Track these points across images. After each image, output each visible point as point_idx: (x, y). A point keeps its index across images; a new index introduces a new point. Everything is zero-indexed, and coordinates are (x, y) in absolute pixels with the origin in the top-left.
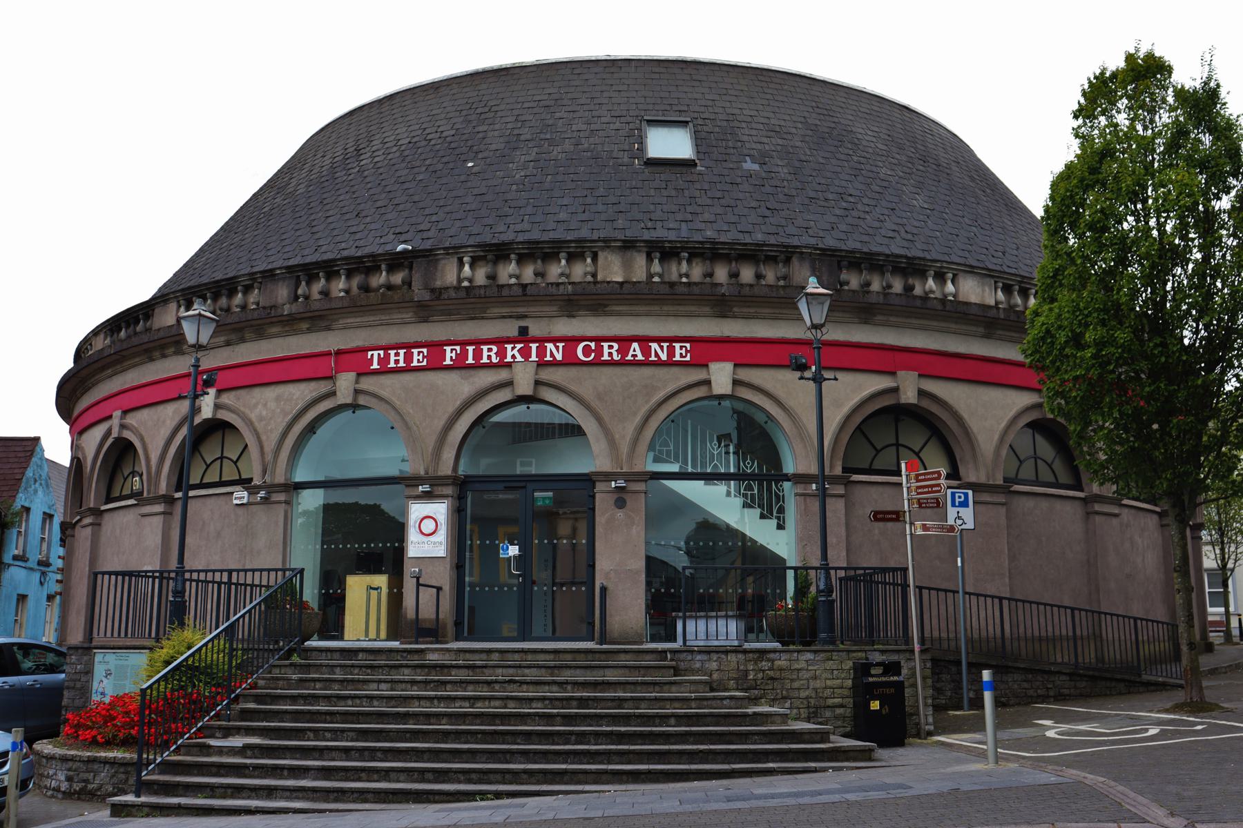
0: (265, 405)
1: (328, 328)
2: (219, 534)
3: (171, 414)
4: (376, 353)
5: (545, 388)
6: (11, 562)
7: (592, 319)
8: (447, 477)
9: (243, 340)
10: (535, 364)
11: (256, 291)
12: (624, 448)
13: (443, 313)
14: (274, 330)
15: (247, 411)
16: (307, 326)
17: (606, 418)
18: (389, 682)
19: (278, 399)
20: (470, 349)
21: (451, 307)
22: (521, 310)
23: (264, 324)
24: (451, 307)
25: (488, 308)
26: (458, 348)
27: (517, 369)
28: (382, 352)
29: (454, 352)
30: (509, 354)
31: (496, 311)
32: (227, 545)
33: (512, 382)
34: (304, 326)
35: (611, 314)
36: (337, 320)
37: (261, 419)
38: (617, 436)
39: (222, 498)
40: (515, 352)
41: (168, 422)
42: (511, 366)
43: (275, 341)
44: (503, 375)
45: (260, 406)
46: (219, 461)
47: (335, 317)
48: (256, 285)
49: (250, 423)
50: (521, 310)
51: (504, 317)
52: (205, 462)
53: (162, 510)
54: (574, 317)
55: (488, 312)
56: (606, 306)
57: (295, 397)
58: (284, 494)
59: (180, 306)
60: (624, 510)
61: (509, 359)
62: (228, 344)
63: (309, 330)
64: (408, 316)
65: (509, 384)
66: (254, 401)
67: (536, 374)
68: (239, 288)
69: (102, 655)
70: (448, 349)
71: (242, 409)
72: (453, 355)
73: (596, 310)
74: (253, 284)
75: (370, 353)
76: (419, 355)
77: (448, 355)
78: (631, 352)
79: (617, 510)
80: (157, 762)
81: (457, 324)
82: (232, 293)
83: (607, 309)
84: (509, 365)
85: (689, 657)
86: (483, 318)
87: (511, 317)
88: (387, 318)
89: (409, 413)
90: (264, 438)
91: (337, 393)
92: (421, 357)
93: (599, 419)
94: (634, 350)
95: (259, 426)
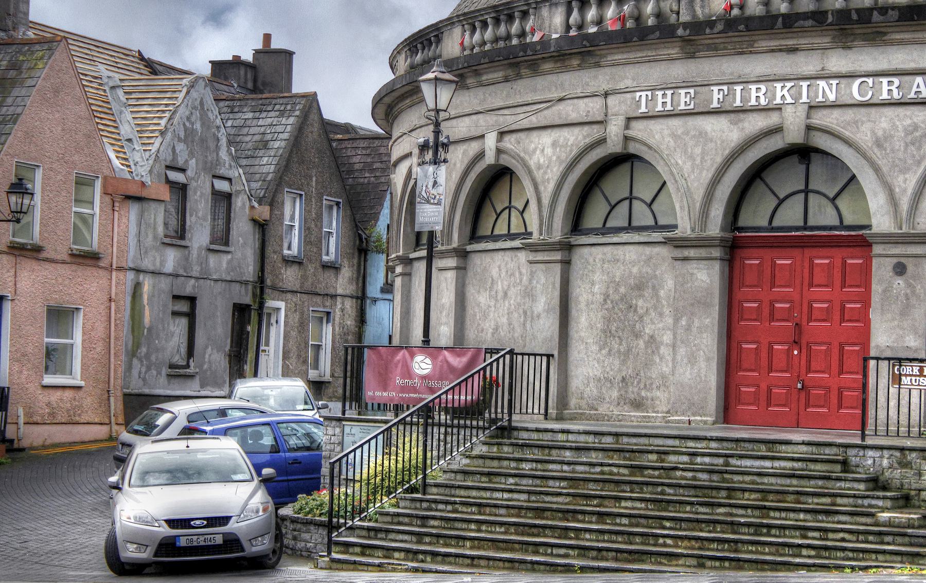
0: (543, 151)
1: (598, 65)
2: (506, 294)
3: (460, 156)
4: (644, 94)
5: (818, 134)
6: (379, 295)
7: (871, 50)
8: (713, 239)
9: (519, 76)
10: (806, 107)
11: (532, 17)
12: (905, 204)
13: (709, 47)
14: (547, 66)
15: (527, 158)
16: (578, 62)
17: (885, 169)
18: (722, 456)
19: (554, 144)
20: (738, 88)
21: (717, 41)
22: (790, 42)
23: (539, 59)
24: (717, 41)
25: (755, 41)
26: (725, 88)
27: (789, 111)
28: (649, 93)
29: (721, 93)
30: (779, 94)
31: (764, 44)
32: (513, 307)
33: (782, 127)
34: (575, 62)
35: (892, 43)
36: (605, 56)
37: (539, 167)
38: (897, 190)
39: (508, 253)
40: (785, 92)
41: (458, 165)
42: (781, 109)
43: (550, 78)
44: (773, 119)
45: (538, 152)
46: (507, 211)
47: (603, 52)
48: (531, 11)
49: (530, 172)
50: (790, 42)
51: (773, 51)
52: (496, 211)
53: (455, 265)
54: (849, 48)
55: (756, 45)
56: (885, 34)
57: (569, 144)
58: (560, 253)
59: (465, 31)
60: (904, 277)
61: (778, 101)
62: (506, 80)
63: (580, 67)
64: (674, 51)
65: (777, 130)
66: (533, 146)
67: (808, 117)
68: (516, 14)
69: (350, 427)
70: (715, 89)
71: (522, 155)
72: (721, 96)
73: (874, 40)
74: (529, 9)
75: (638, 94)
76: (686, 97)
77: (716, 96)
78: (914, 89)
79: (896, 277)
80: (348, 526)
81: (724, 59)
82: (510, 18)
83: (885, 38)
84: (779, 109)
85: (861, 453)
86: (751, 52)
87: (781, 50)
88: (654, 54)
89: (677, 164)
90: (542, 188)
91: (608, 140)
92: (688, 100)
93: (877, 170)
94: (918, 86)
95: (538, 175)
